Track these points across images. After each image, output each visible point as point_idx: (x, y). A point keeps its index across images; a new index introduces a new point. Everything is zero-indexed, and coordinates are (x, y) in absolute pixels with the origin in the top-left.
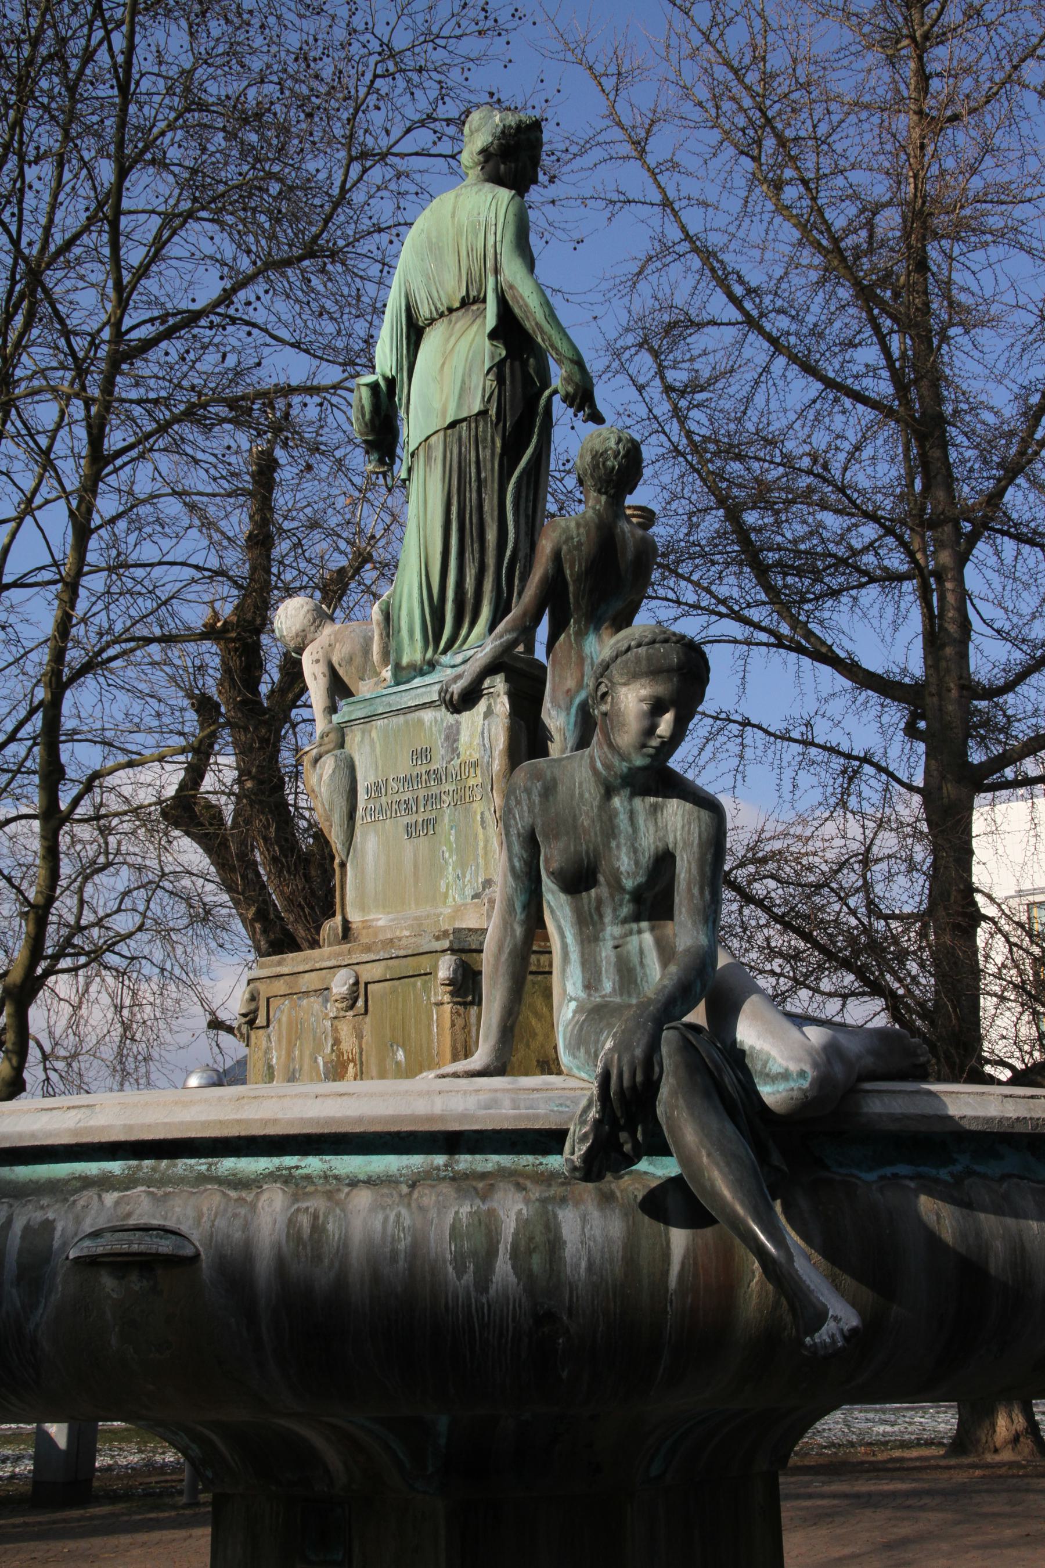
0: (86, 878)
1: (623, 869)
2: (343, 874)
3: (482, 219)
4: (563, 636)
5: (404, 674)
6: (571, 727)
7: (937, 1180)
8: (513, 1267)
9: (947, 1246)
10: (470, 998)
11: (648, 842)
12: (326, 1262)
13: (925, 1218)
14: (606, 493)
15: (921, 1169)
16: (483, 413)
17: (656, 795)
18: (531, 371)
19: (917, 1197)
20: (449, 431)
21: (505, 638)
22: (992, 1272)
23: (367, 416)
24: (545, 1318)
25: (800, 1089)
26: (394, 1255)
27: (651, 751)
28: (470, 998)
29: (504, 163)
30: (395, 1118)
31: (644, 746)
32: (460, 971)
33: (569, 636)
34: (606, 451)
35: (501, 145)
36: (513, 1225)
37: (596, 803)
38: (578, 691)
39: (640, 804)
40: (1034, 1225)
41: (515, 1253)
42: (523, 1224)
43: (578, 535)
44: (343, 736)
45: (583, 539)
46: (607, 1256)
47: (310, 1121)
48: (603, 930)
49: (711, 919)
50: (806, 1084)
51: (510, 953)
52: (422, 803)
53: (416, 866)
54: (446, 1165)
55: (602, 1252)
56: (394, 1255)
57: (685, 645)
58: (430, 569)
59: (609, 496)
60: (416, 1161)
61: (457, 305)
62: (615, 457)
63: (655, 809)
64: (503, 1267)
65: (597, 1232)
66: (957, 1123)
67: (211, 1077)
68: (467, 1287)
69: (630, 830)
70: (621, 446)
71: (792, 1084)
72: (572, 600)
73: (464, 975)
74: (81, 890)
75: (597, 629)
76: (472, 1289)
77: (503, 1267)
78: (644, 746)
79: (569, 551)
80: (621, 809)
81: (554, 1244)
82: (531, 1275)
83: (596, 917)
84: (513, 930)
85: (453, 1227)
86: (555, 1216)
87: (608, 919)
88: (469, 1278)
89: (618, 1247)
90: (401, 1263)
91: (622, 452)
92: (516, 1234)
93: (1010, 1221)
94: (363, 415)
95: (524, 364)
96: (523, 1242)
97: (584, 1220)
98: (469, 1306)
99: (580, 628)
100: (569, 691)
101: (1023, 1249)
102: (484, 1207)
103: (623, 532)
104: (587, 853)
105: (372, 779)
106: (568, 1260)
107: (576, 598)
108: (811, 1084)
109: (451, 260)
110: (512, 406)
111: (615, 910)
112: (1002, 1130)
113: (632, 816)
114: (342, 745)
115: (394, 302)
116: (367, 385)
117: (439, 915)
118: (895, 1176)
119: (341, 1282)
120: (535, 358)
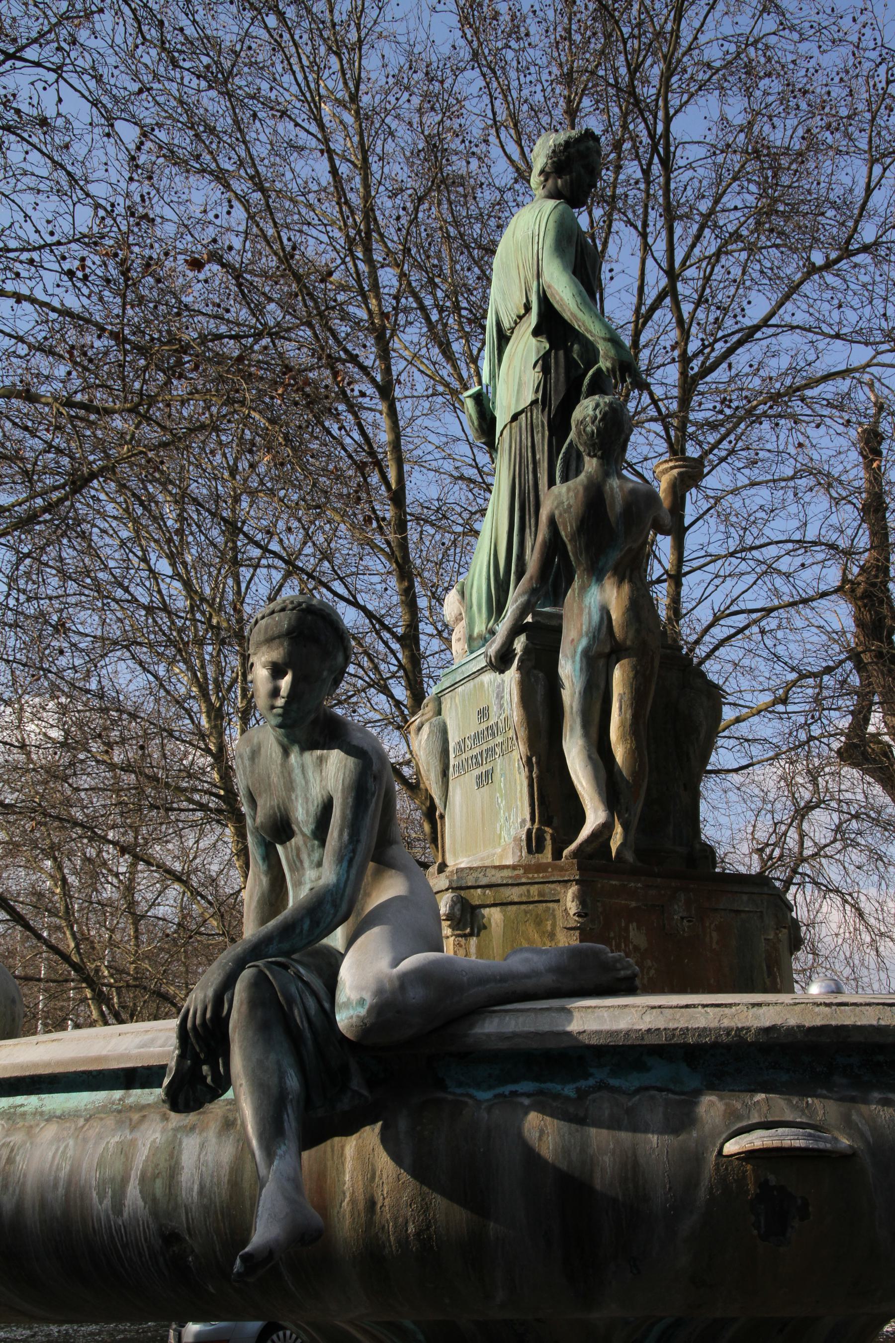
0: (803, 817)
1: (300, 819)
2: (443, 825)
3: (530, 233)
4: (570, 591)
5: (475, 644)
6: (578, 673)
7: (556, 1096)
8: (141, 1192)
9: (546, 1162)
10: (468, 930)
11: (316, 794)
12: (11, 1189)
13: (526, 1133)
14: (595, 456)
15: (549, 1086)
16: (534, 402)
17: (323, 749)
18: (575, 356)
19: (526, 1113)
20: (514, 424)
21: (519, 602)
22: (598, 1187)
23: (476, 423)
24: (171, 1238)
25: (358, 1016)
26: (56, 1179)
27: (280, 711)
28: (468, 930)
29: (560, 177)
30: (74, 1061)
31: (273, 707)
32: (458, 906)
33: (574, 591)
34: (585, 418)
35: (554, 162)
36: (146, 1152)
37: (279, 762)
38: (579, 640)
39: (310, 757)
40: (654, 1138)
41: (143, 1179)
42: (155, 1150)
43: (568, 499)
44: (440, 704)
45: (572, 502)
46: (215, 1180)
47: (22, 1067)
48: (303, 875)
49: (347, 858)
50: (362, 1012)
51: (258, 901)
52: (484, 755)
53: (483, 814)
54: (120, 1100)
55: (212, 1176)
56: (56, 1179)
57: (302, 610)
58: (499, 548)
59: (599, 458)
60: (99, 1097)
61: (523, 312)
62: (593, 422)
63: (321, 760)
64: (133, 1191)
65: (210, 1158)
66: (576, 1039)
67: (830, 986)
68: (106, 1210)
69: (303, 782)
70: (597, 412)
71: (351, 1012)
72: (572, 558)
73: (463, 910)
74: (800, 826)
75: (600, 580)
76: (110, 1212)
77: (133, 1191)
78: (273, 707)
79: (561, 515)
80: (295, 764)
81: (174, 1170)
82: (154, 1200)
83: (298, 864)
84: (261, 880)
85: (102, 1155)
86: (180, 1143)
87: (306, 864)
88: (107, 1202)
89: (225, 1171)
90: (61, 1191)
91: (599, 416)
92: (146, 1161)
93: (625, 1136)
94: (473, 423)
95: (568, 352)
96: (150, 1169)
97: (202, 1146)
98: (110, 1227)
99: (583, 581)
100: (573, 640)
101: (636, 1164)
102: (129, 1137)
103: (612, 488)
104: (279, 808)
105: (457, 740)
106: (184, 1184)
107: (575, 555)
108: (369, 1011)
109: (514, 273)
110: (556, 391)
111: (309, 855)
112: (629, 1043)
113: (303, 768)
114: (439, 712)
115: (490, 322)
116: (469, 397)
117: (494, 855)
118: (514, 1094)
119: (19, 1209)
120: (579, 343)
